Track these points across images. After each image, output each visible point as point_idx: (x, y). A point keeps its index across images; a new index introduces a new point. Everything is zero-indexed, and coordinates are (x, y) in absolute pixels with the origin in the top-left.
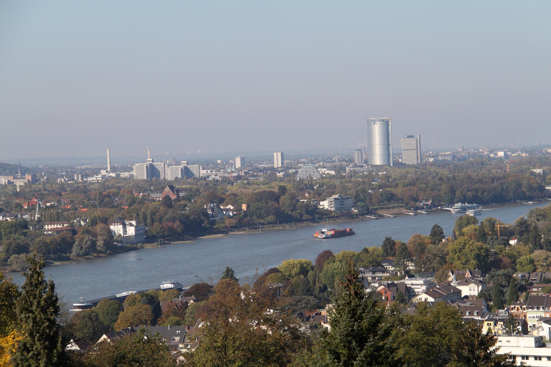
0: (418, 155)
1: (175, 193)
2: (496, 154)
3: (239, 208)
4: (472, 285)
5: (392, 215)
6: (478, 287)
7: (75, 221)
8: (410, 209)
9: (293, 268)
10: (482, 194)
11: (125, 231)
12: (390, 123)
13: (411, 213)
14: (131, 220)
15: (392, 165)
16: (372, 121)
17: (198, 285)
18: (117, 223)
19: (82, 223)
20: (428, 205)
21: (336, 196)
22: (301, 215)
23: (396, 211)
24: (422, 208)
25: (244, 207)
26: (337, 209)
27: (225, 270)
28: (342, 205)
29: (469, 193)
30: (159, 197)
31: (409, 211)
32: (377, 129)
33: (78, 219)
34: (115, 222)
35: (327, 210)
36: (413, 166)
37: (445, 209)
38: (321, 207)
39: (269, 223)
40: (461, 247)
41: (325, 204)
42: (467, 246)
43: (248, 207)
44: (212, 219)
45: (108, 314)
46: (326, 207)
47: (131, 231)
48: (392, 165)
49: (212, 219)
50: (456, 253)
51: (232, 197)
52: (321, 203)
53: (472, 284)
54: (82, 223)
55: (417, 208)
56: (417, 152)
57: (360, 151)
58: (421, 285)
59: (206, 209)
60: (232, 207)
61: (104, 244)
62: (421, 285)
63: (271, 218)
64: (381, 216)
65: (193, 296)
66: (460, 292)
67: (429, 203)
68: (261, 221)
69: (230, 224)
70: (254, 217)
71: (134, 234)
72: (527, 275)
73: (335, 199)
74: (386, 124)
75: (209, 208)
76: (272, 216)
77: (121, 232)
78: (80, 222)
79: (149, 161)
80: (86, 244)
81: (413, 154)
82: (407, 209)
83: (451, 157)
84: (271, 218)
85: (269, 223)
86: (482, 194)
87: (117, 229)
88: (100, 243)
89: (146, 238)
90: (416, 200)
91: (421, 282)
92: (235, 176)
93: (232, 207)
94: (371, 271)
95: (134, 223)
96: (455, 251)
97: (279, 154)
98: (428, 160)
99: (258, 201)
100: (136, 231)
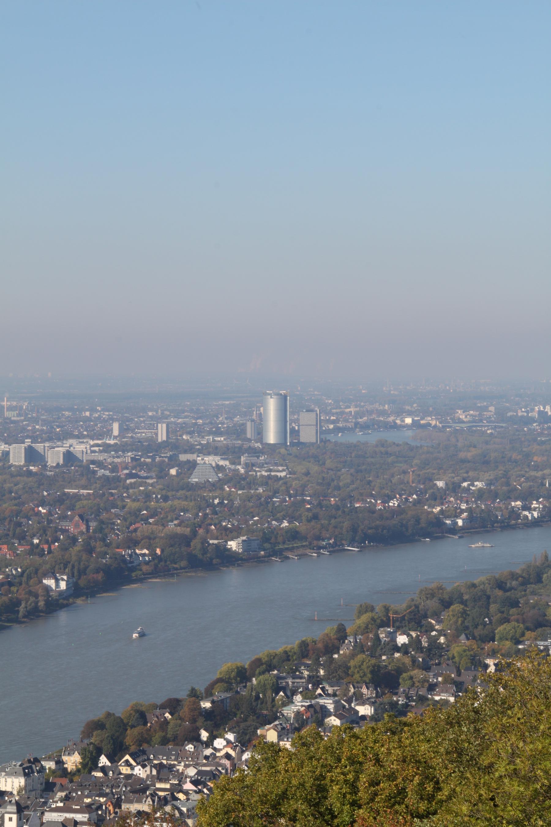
0: (317, 419)
1: (85, 522)
2: (404, 421)
3: (153, 553)
4: (367, 707)
5: (296, 556)
6: (371, 707)
7: (7, 570)
8: (313, 549)
9: (232, 672)
10: (382, 531)
11: (57, 585)
12: (288, 398)
13: (314, 554)
14: (63, 575)
15: (288, 444)
16: (269, 394)
17: (171, 699)
18: (50, 577)
19: (14, 572)
20: (330, 544)
21: (244, 538)
22: (211, 559)
23: (301, 551)
24: (324, 548)
25: (158, 551)
26: (244, 551)
27: (190, 689)
28: (249, 546)
29: (369, 531)
30: (68, 526)
31: (312, 551)
32: (272, 406)
33: (10, 568)
34: (45, 575)
35: (235, 552)
36: (312, 444)
37: (346, 548)
38: (229, 547)
39: (181, 568)
40: (360, 664)
41: (233, 545)
42: (365, 663)
43: (162, 551)
44: (130, 565)
45: (113, 726)
46: (234, 548)
47: (63, 585)
48: (288, 444)
49: (130, 565)
50: (356, 668)
51: (147, 540)
52: (229, 543)
53: (367, 706)
54: (14, 572)
55: (320, 548)
56: (317, 427)
57: (253, 423)
58: (331, 703)
59: (124, 555)
60: (147, 552)
61: (45, 604)
62: (331, 703)
63: (183, 563)
64: (288, 558)
65: (168, 710)
66: (357, 712)
67: (331, 541)
68: (175, 566)
69: (147, 570)
70: (168, 563)
71: (65, 588)
72: (407, 690)
73: (243, 541)
74: (284, 399)
75: (125, 552)
76: (185, 562)
77: (53, 587)
78: (12, 571)
79: (28, 442)
80: (30, 605)
81: (313, 430)
82: (311, 549)
83: (353, 424)
84: (183, 563)
85: (181, 568)
86: (382, 531)
87: (50, 582)
88: (41, 604)
89: (77, 591)
90: (319, 538)
91: (331, 701)
92: (127, 474)
93: (147, 552)
94: (291, 677)
95: (65, 577)
96: (355, 667)
97: (164, 426)
98: (328, 427)
99: (172, 546)
100: (67, 585)
